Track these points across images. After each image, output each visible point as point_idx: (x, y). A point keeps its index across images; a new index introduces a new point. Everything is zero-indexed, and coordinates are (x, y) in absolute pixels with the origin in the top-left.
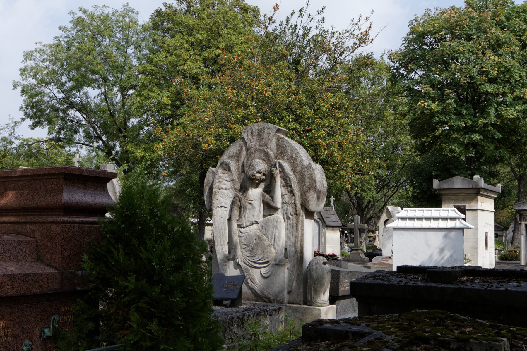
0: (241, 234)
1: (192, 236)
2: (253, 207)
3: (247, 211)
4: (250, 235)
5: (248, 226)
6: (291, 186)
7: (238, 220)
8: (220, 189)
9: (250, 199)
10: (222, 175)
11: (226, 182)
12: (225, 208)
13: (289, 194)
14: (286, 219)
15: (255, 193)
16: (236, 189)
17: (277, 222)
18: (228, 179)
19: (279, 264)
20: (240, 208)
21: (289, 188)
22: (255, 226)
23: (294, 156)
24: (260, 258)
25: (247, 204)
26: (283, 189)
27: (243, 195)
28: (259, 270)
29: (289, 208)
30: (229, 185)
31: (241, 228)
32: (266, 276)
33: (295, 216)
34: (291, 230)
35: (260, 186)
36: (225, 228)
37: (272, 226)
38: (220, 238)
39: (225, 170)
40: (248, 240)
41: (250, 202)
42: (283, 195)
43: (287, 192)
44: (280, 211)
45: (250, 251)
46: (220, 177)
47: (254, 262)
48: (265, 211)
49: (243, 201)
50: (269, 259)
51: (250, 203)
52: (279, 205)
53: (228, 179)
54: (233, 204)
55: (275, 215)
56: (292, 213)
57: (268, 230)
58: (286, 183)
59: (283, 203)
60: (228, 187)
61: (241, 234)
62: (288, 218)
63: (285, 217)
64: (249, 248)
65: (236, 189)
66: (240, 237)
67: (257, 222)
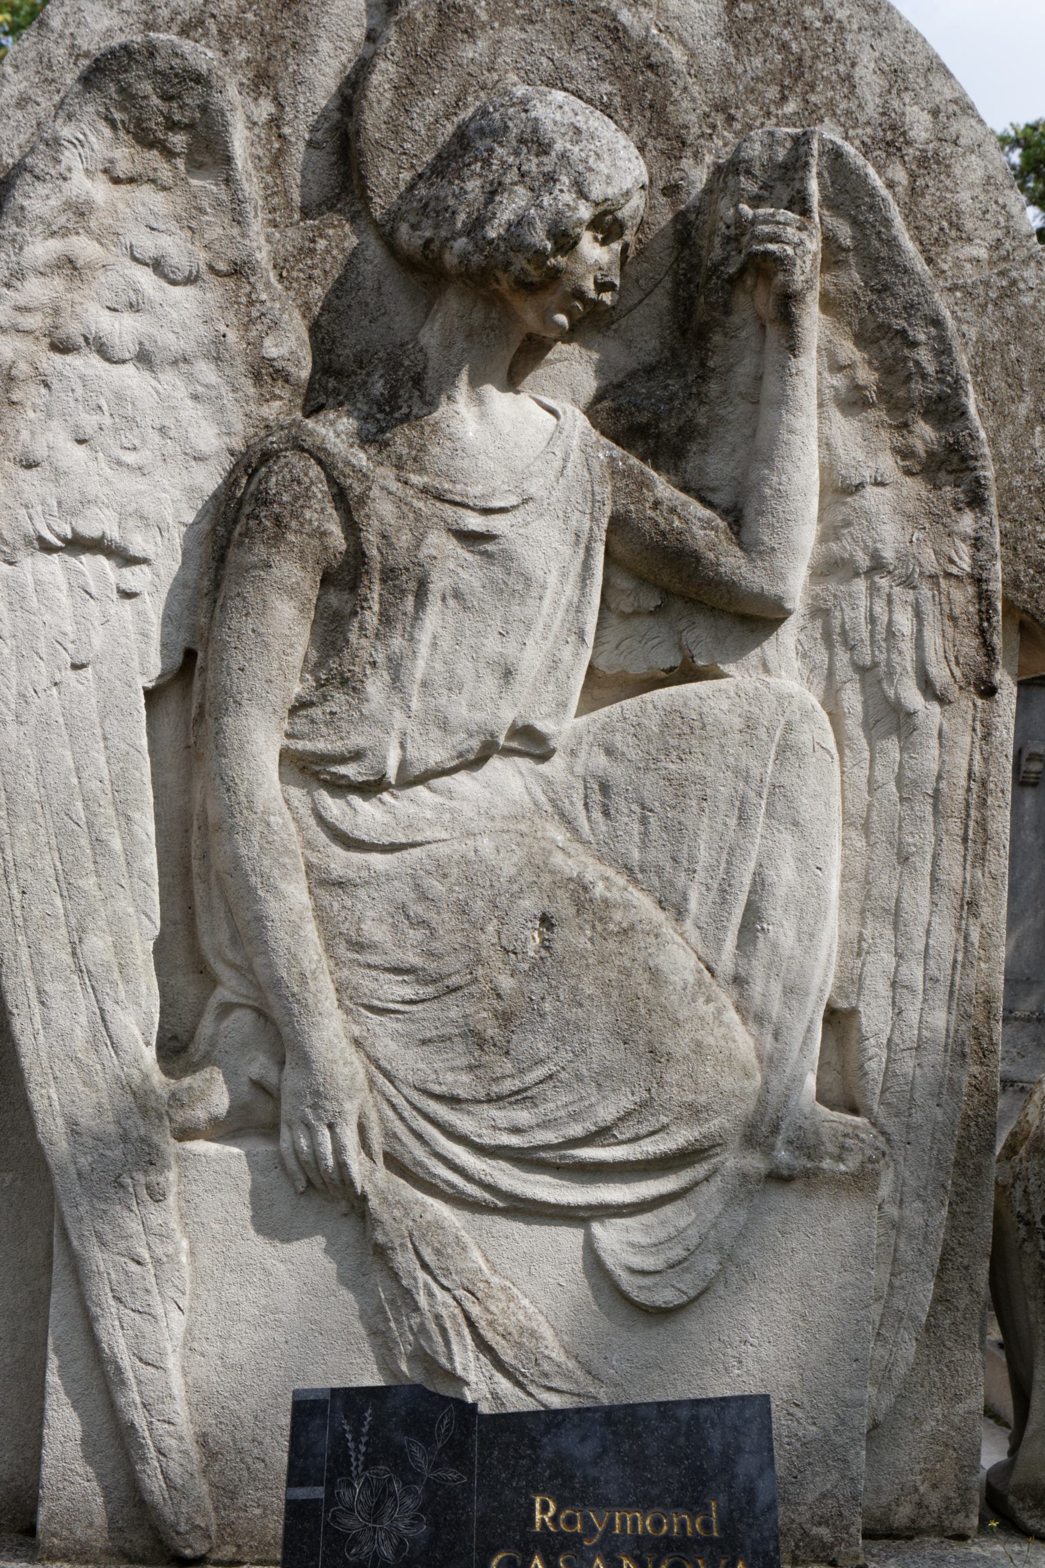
0: (340, 861)
1: (911, 1204)
2: (512, 580)
3: (433, 619)
4: (472, 873)
5: (424, 778)
6: (945, 409)
7: (300, 707)
8: (62, 347)
9: (475, 491)
10: (100, 191)
11: (146, 279)
12: (126, 559)
13: (914, 487)
14: (853, 726)
15: (525, 441)
16: (266, 373)
17: (785, 749)
18: (175, 247)
19: (781, 1163)
20: (344, 578)
21: (925, 434)
22: (509, 777)
23: (920, 126)
24: (606, 1113)
25: (439, 543)
26: (845, 430)
27: (372, 437)
28: (570, 1238)
29: (905, 622)
30: (183, 313)
31: (341, 787)
32: (665, 1296)
33: (967, 703)
34: (922, 837)
35: (539, 375)
36: (120, 783)
37: (724, 788)
38: (68, 890)
39: (145, 139)
40: (445, 920)
41: (474, 522)
42: (839, 489)
43: (888, 464)
44: (789, 634)
45: (479, 1040)
46: (80, 211)
47: (525, 1159)
48: (616, 630)
49: (382, 509)
50: (714, 1124)
51: (469, 538)
52: (796, 586)
53: (175, 247)
54: (233, 526)
55: (740, 677)
56: (940, 673)
57: (676, 831)
58: (894, 371)
59: (831, 568)
60: (169, 341)
61: (340, 861)
62: (891, 720)
63: (852, 699)
64: (454, 1010)
65: (266, 373)
66: (322, 882)
67: (531, 743)
